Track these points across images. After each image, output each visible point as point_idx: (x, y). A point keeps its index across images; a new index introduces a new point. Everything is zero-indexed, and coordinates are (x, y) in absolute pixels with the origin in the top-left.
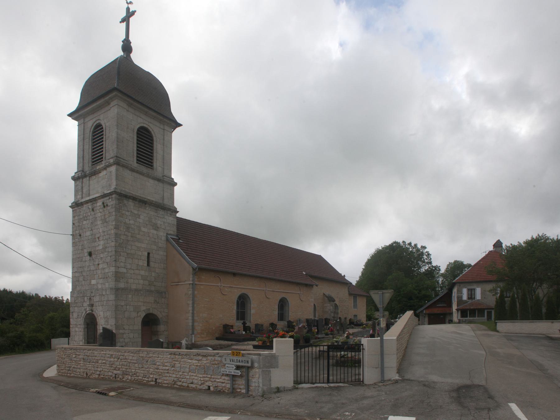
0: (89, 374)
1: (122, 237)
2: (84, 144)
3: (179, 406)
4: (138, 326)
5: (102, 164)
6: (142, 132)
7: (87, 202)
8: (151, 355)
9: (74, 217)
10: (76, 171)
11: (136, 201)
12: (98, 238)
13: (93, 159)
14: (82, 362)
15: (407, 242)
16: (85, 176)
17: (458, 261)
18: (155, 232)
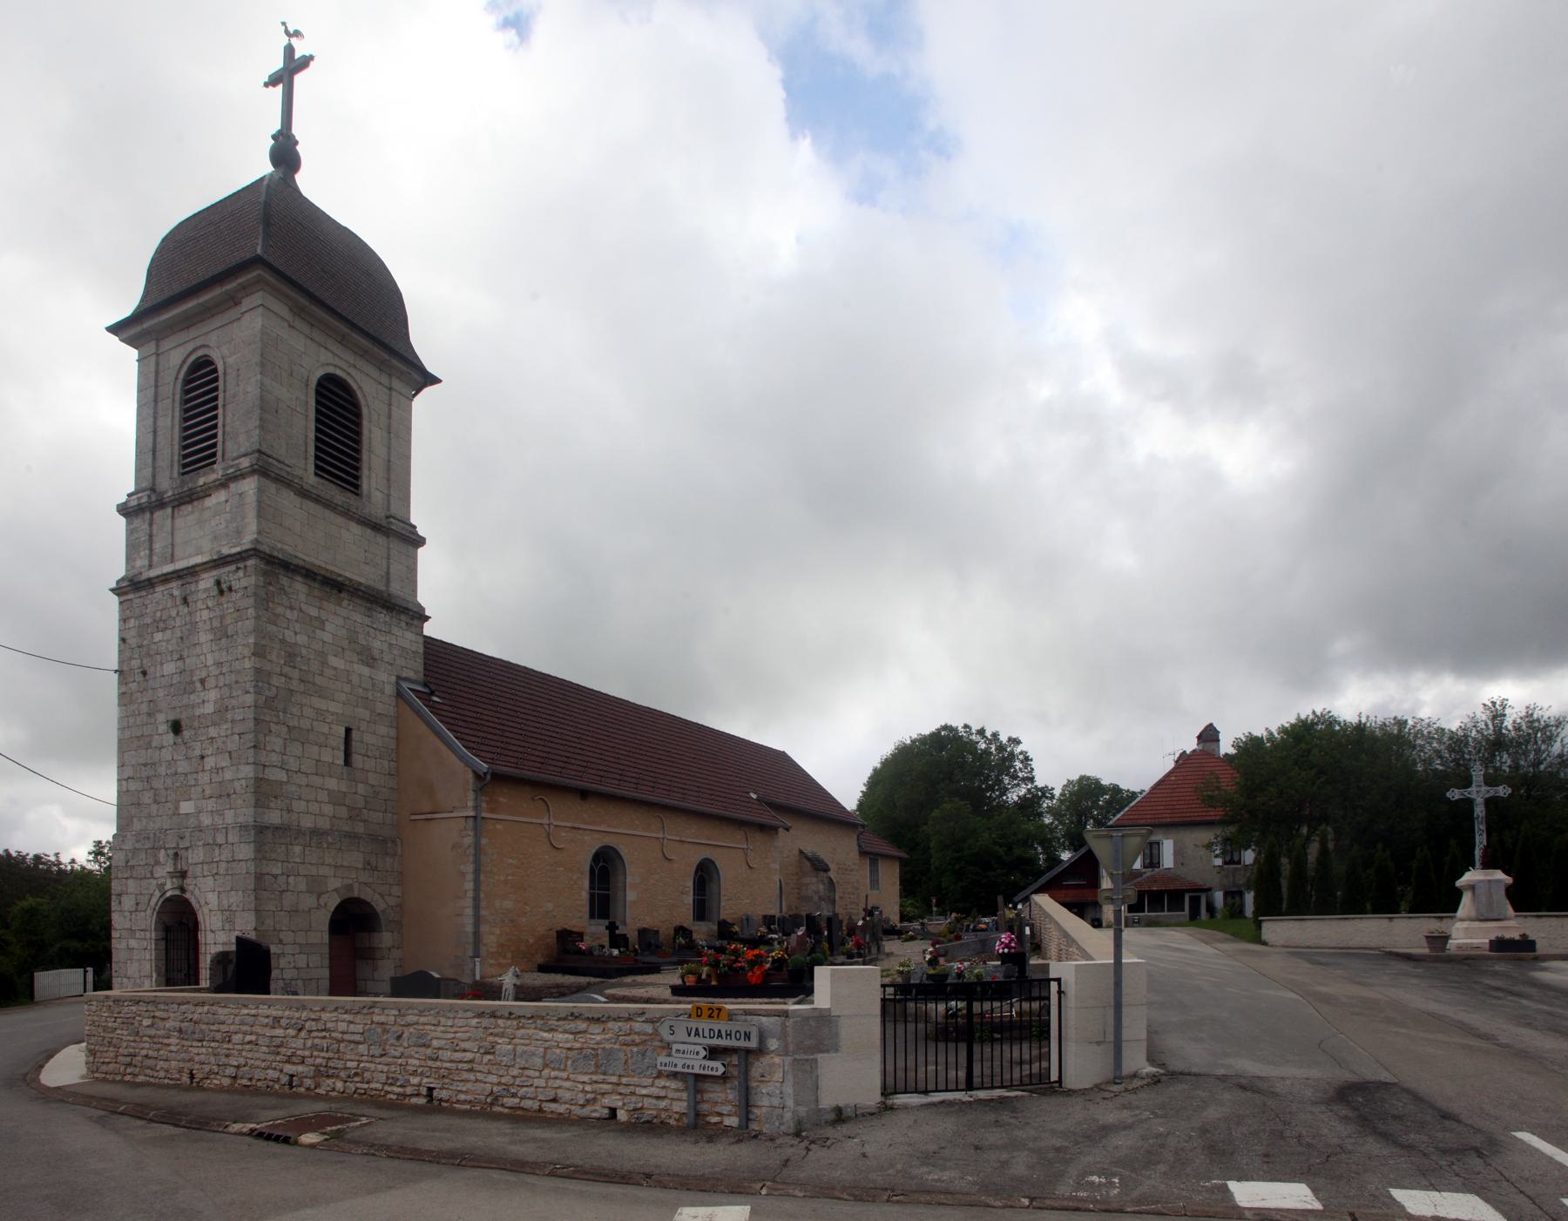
0: (199, 1076)
1: (277, 681)
2: (155, 412)
3: (552, 1174)
4: (320, 934)
5: (213, 471)
6: (330, 391)
7: (166, 579)
8: (411, 1019)
9: (124, 620)
10: (132, 489)
11: (314, 580)
12: (202, 681)
13: (185, 457)
14: (173, 1041)
15: (975, 727)
16: (161, 505)
17: (1088, 778)
18: (366, 671)
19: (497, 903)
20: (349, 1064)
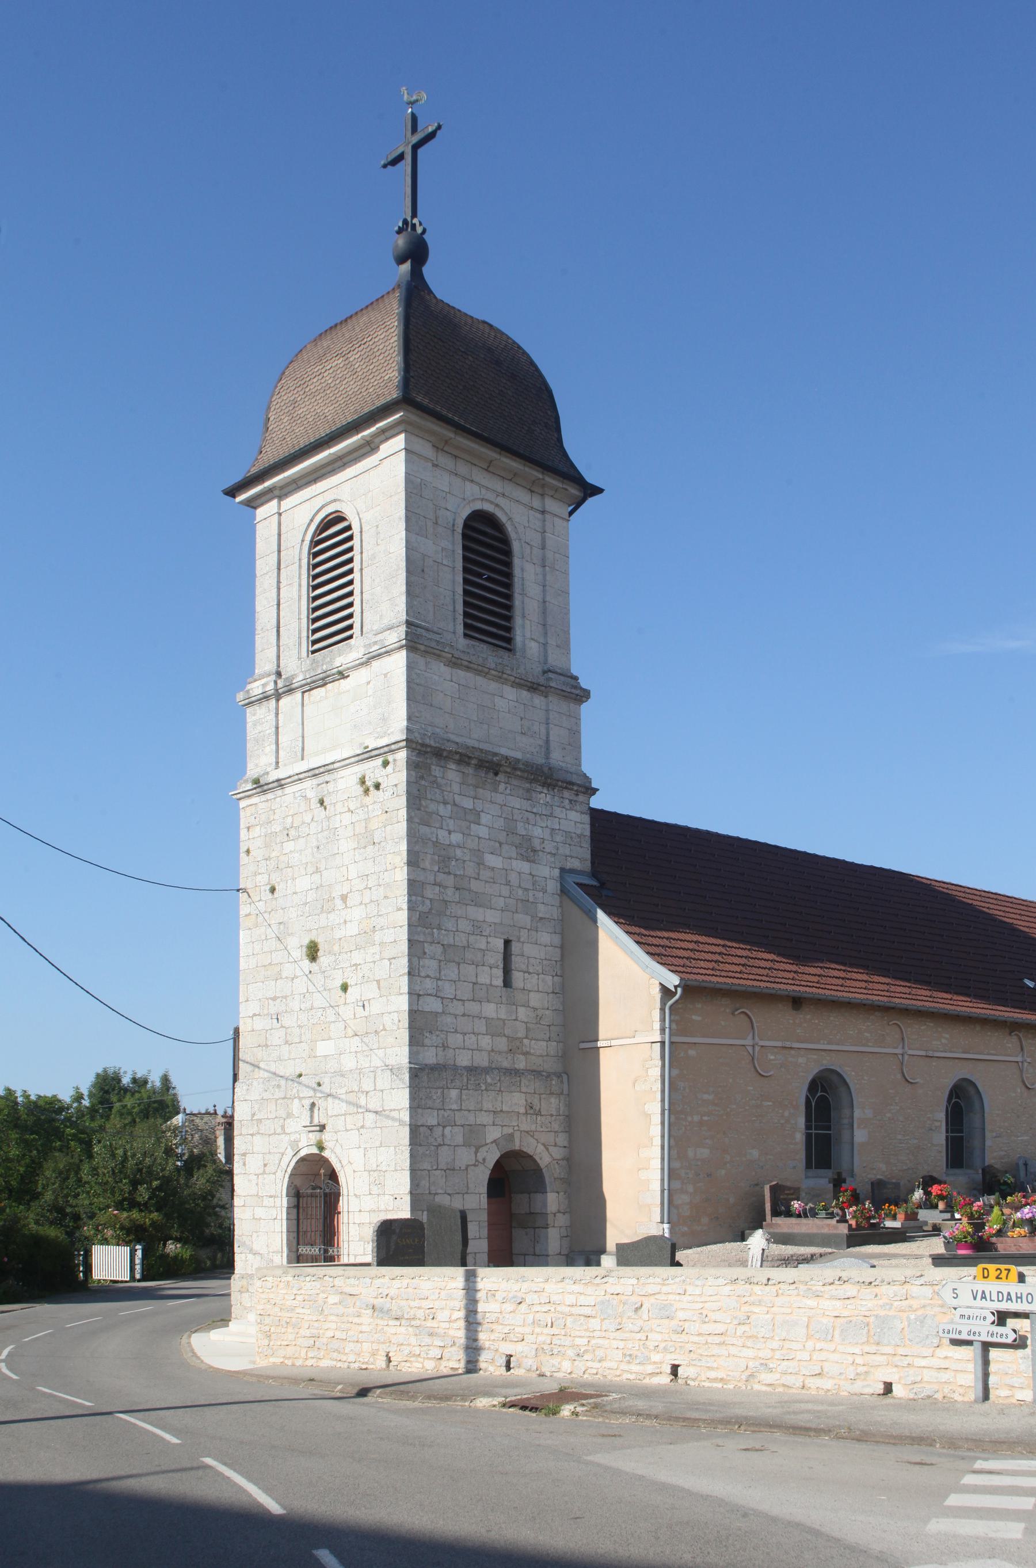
7: (298, 778)
12: (344, 898)
18: (525, 867)
19: (691, 1153)
20: (578, 1341)
